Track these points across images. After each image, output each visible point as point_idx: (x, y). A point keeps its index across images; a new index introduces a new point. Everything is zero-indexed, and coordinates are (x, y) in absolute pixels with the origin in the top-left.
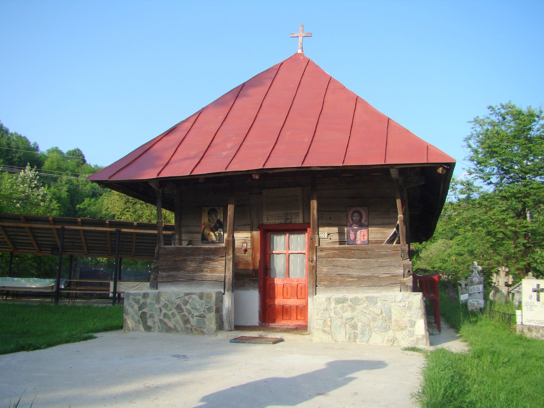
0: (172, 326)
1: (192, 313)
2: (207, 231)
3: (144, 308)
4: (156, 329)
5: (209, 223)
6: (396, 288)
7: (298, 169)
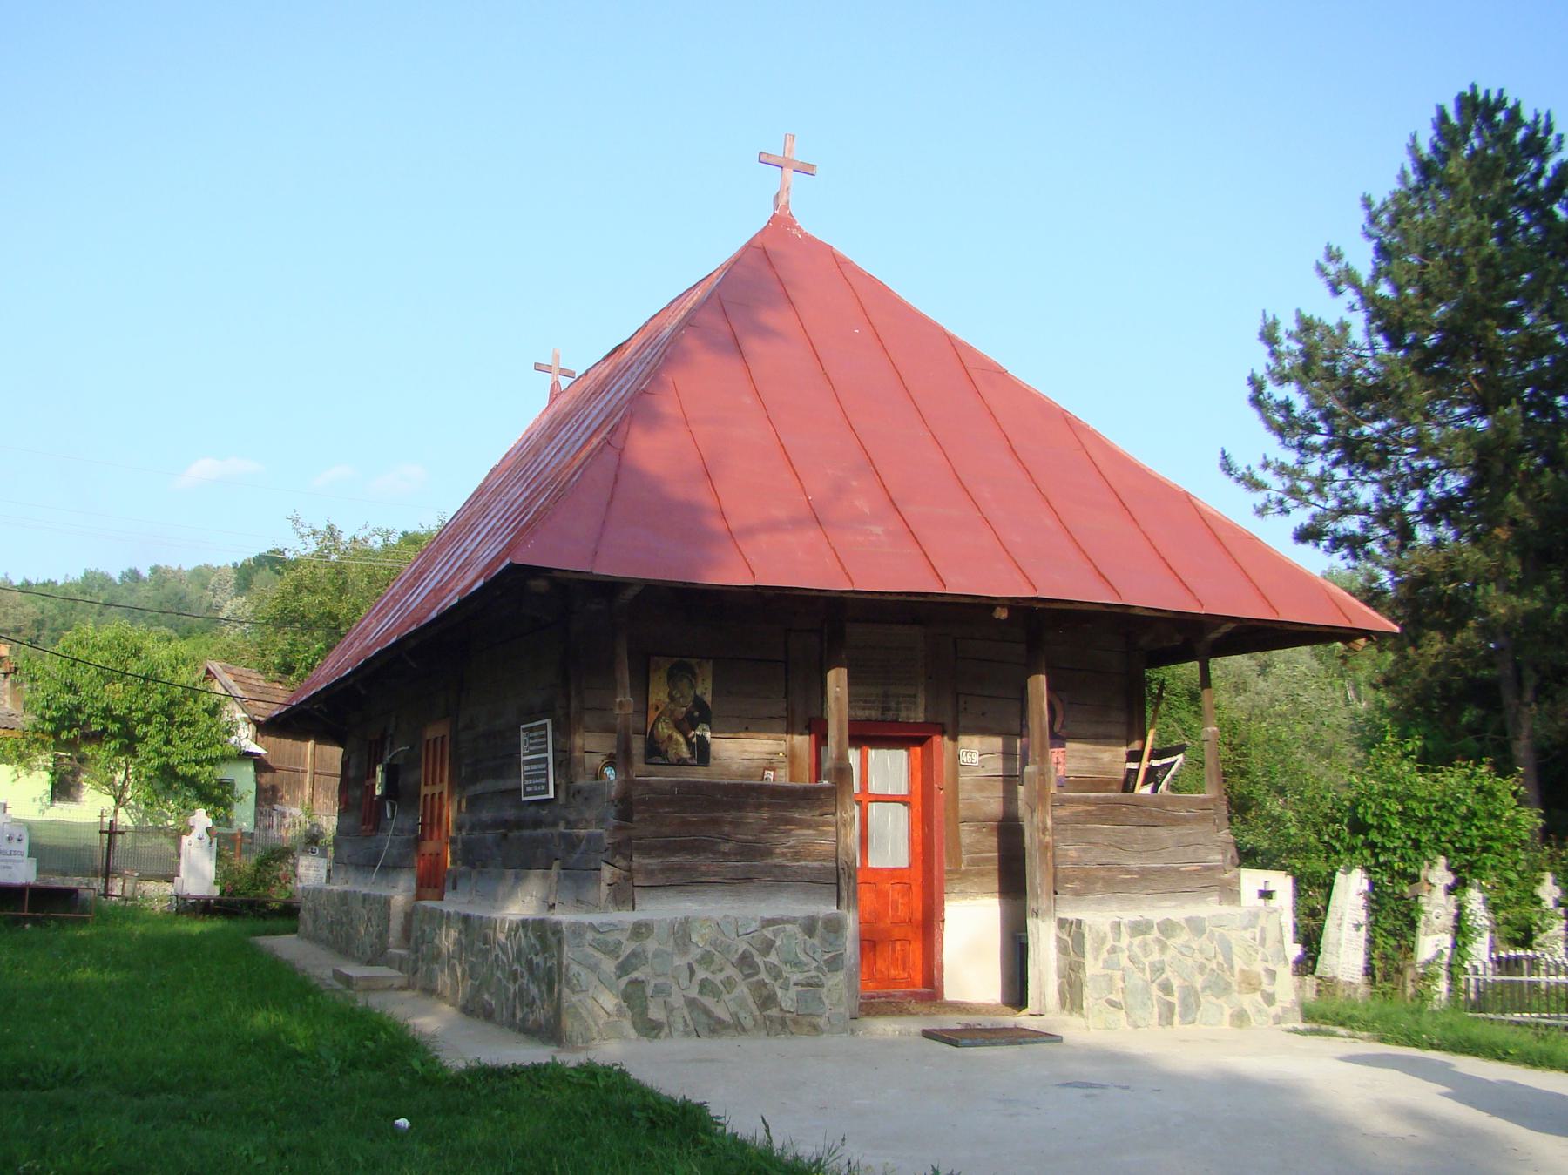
0: (726, 1017)
1: (785, 974)
2: (664, 730)
3: (636, 969)
4: (676, 1030)
5: (672, 706)
6: (1212, 896)
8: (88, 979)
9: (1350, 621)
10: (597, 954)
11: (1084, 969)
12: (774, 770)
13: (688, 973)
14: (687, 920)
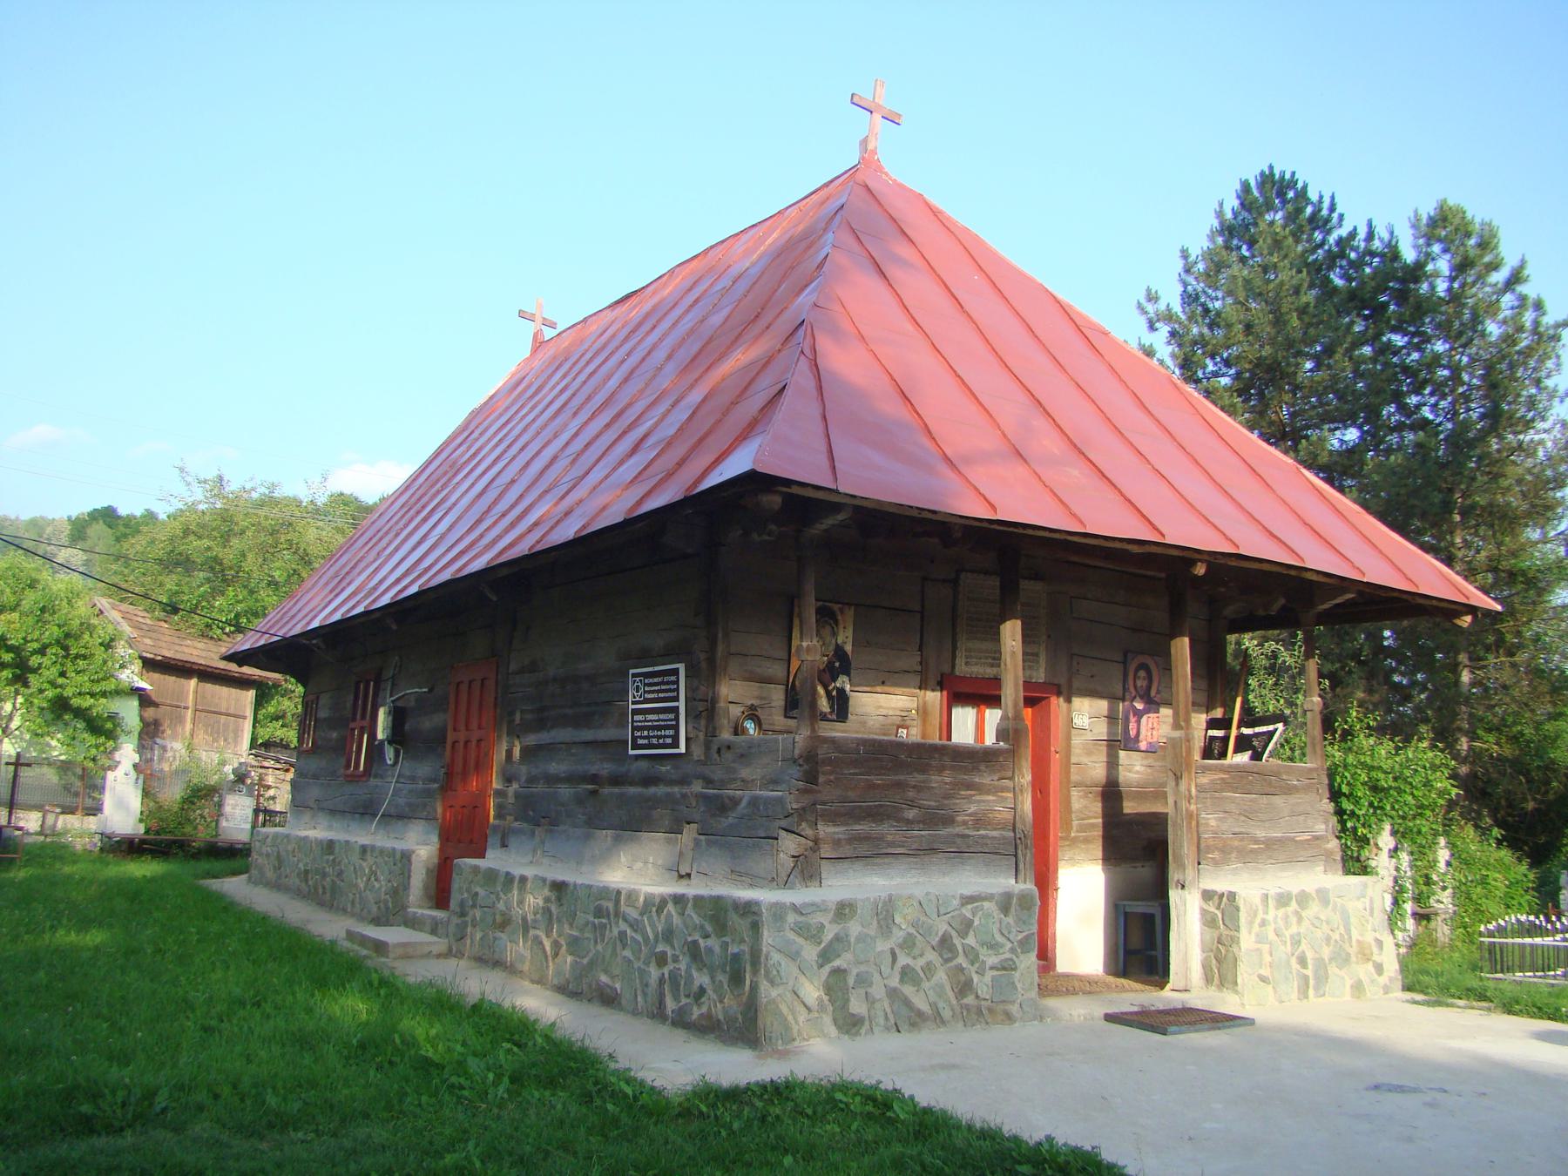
1: (981, 957)
4: (877, 1025)
8: (71, 942)
9: (1468, 598)
11: (1238, 943)
12: (907, 728)
14: (890, 898)
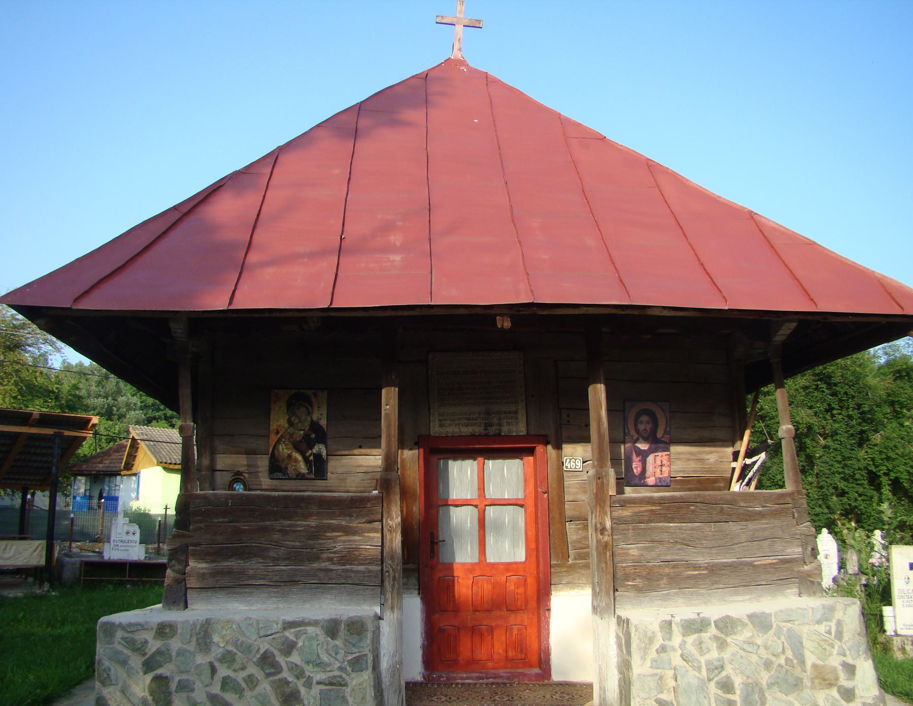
1: (307, 674)
2: (284, 450)
3: (161, 666)
5: (291, 430)
6: (791, 588)
7: (614, 311)
9: (902, 309)
10: (126, 651)
13: (210, 671)
